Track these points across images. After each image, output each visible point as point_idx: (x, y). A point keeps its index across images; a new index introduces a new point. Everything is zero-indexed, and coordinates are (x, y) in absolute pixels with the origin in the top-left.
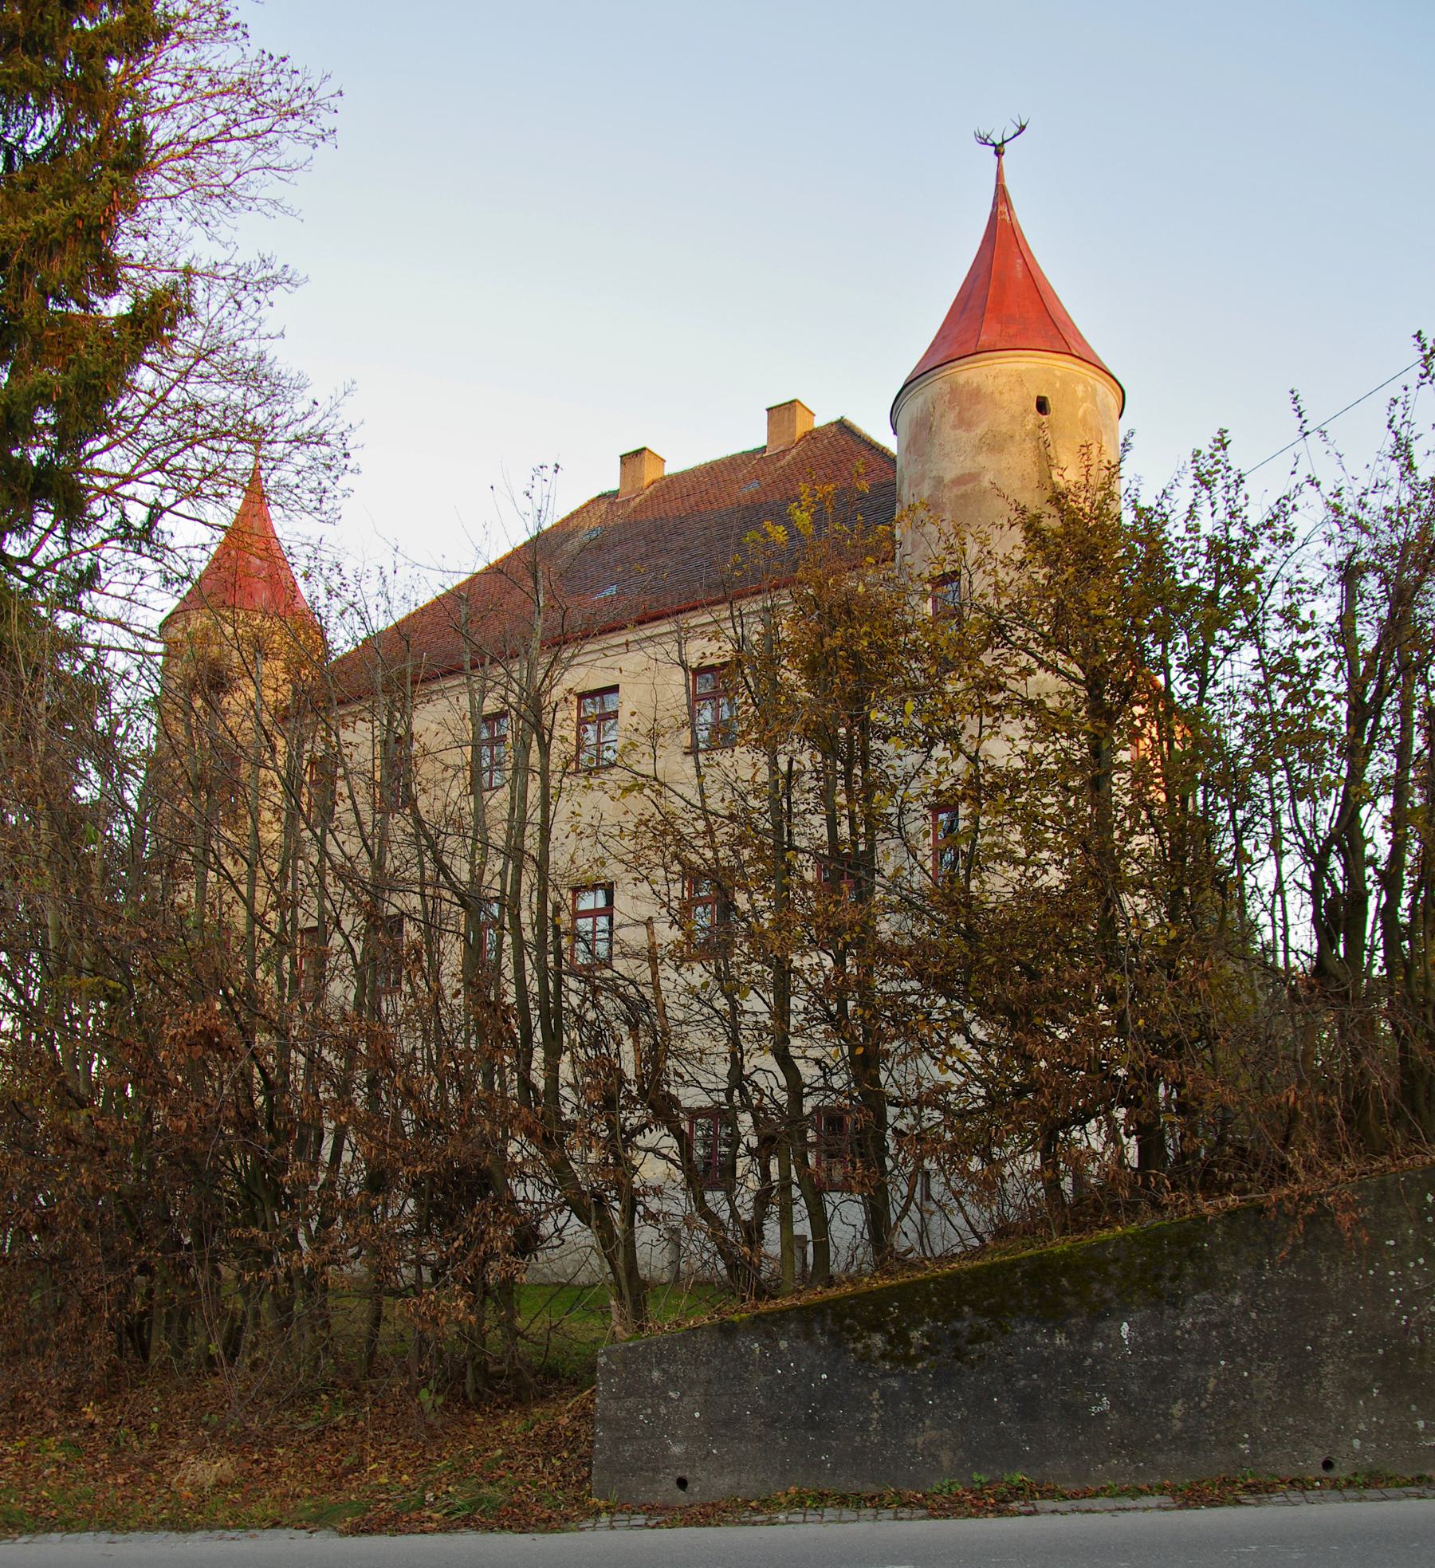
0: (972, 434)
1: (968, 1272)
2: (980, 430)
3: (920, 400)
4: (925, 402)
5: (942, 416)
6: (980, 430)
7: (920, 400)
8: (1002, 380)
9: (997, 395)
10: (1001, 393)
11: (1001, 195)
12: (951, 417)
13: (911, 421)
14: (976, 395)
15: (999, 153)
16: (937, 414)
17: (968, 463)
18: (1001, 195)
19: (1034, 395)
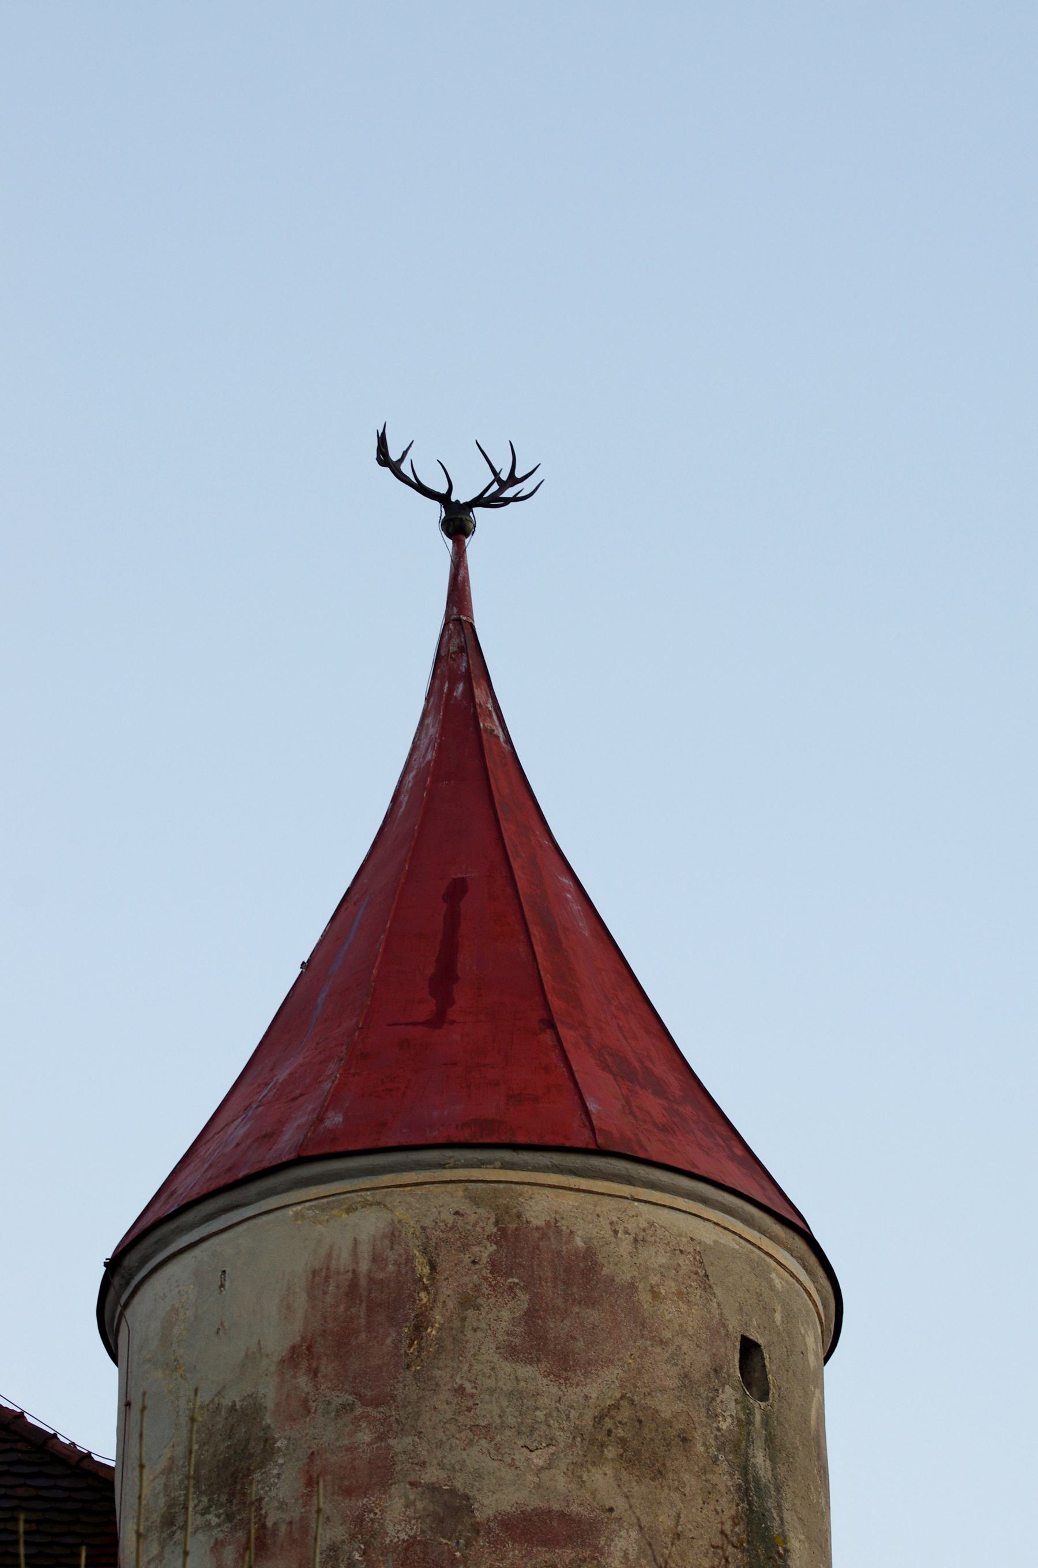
0: (574, 1394)
1: (810, 1416)
2: (599, 1388)
3: (369, 1224)
4: (393, 1236)
5: (467, 1302)
6: (599, 1388)
7: (369, 1224)
8: (657, 1258)
9: (644, 1297)
10: (655, 1295)
11: (460, 667)
12: (502, 1316)
13: (319, 1278)
14: (582, 1274)
15: (457, 523)
16: (448, 1291)
17: (561, 1483)
18: (460, 667)
19: (734, 1326)
